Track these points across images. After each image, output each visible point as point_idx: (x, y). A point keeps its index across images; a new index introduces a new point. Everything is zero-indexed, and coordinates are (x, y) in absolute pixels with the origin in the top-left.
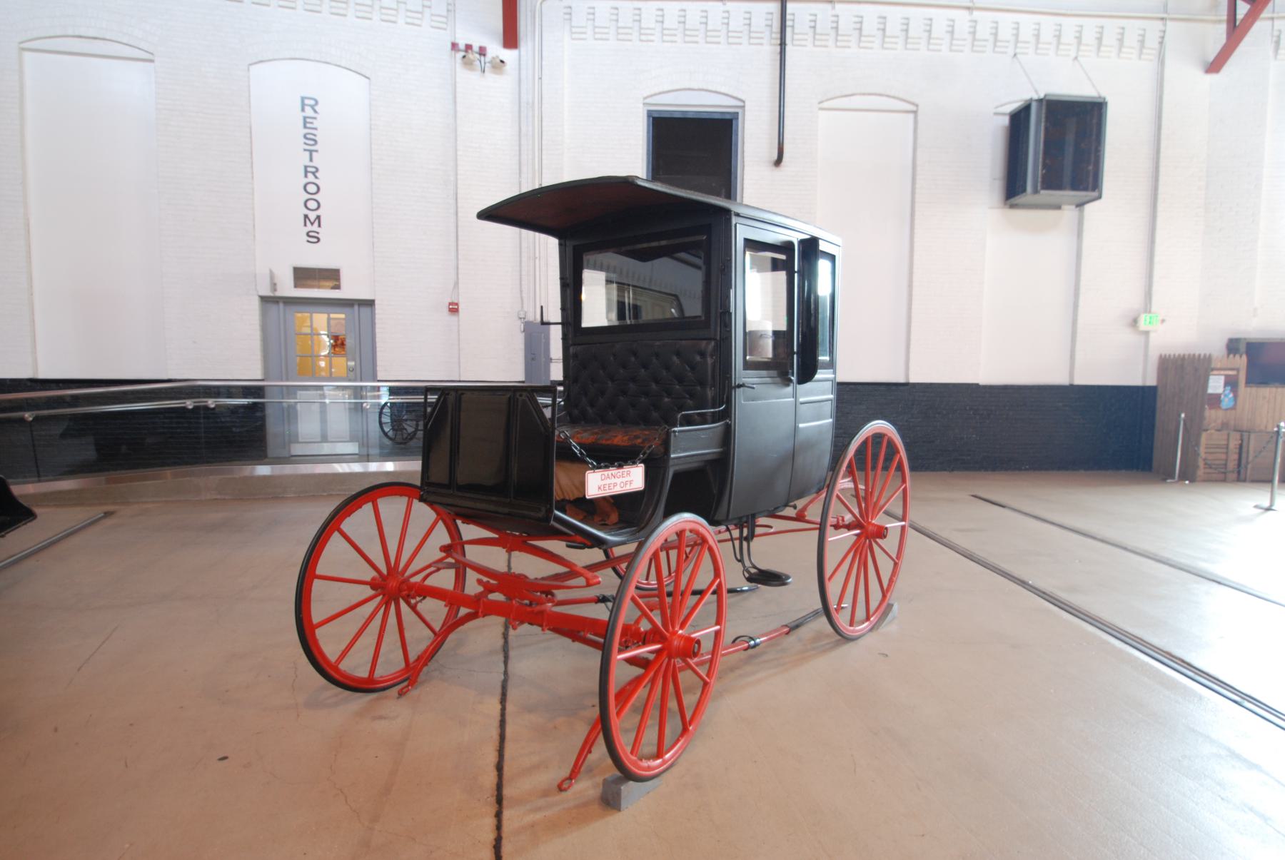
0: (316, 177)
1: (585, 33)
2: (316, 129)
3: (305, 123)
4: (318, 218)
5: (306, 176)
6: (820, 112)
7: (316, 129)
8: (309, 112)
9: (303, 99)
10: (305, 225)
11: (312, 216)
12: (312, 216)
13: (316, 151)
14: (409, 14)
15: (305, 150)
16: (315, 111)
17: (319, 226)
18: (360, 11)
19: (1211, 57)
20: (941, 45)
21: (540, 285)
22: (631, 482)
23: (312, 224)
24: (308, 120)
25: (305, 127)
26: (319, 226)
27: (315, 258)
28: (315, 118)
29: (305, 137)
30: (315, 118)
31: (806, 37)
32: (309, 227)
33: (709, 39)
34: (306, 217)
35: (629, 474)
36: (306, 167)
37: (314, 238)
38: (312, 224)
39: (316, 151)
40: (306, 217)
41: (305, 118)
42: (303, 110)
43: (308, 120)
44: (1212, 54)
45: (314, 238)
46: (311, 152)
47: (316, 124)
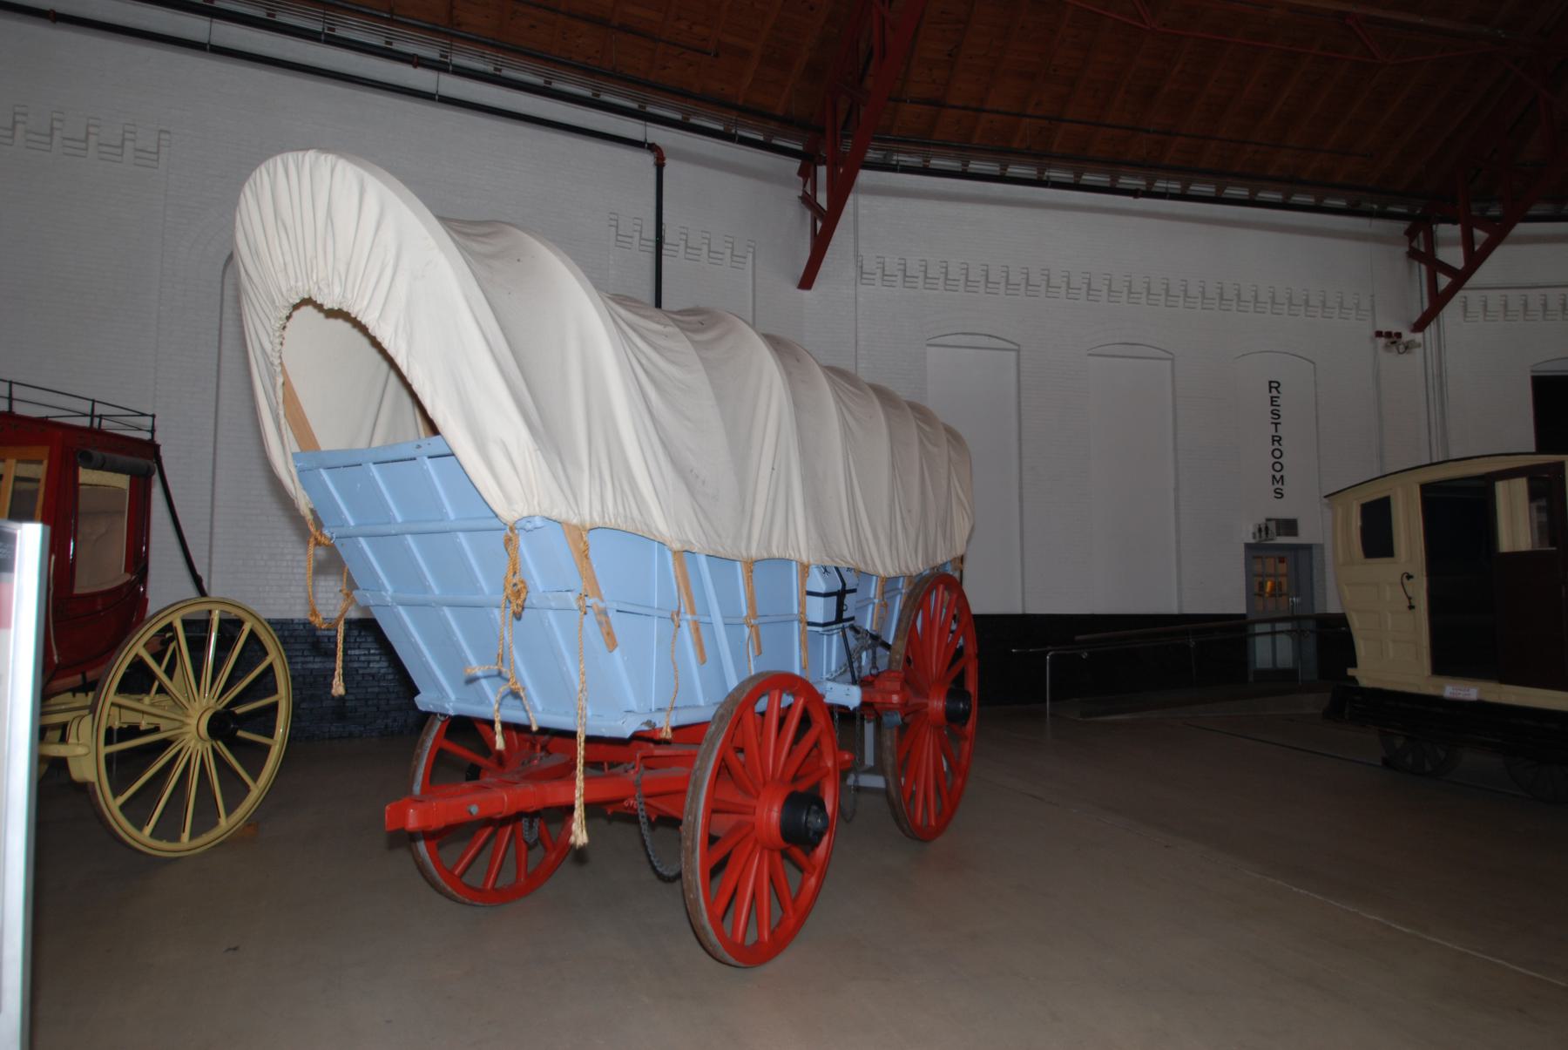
0: (1280, 445)
1: (1018, 290)
2: (1278, 406)
3: (1272, 401)
4: (1282, 477)
5: (1273, 444)
6: (928, 348)
7: (1278, 406)
8: (1274, 392)
9: (1270, 382)
10: (1273, 483)
11: (1278, 476)
12: (1278, 476)
13: (1279, 423)
14: (629, 246)
15: (1272, 423)
16: (1279, 392)
17: (1283, 484)
18: (629, 243)
19: (1415, 319)
20: (1140, 298)
21: (843, 524)
22: (1469, 695)
23: (1278, 482)
24: (1274, 399)
25: (1272, 405)
26: (1283, 484)
27: (1282, 510)
28: (1278, 397)
29: (1272, 413)
30: (1278, 397)
31: (1213, 301)
32: (1277, 486)
33: (948, 287)
34: (1274, 477)
35: (1468, 690)
36: (1273, 436)
37: (1279, 494)
38: (1278, 482)
39: (1279, 423)
40: (1274, 477)
41: (1272, 397)
42: (1270, 392)
43: (1274, 399)
44: (1416, 316)
45: (1279, 494)
46: (1276, 424)
47: (1279, 402)
